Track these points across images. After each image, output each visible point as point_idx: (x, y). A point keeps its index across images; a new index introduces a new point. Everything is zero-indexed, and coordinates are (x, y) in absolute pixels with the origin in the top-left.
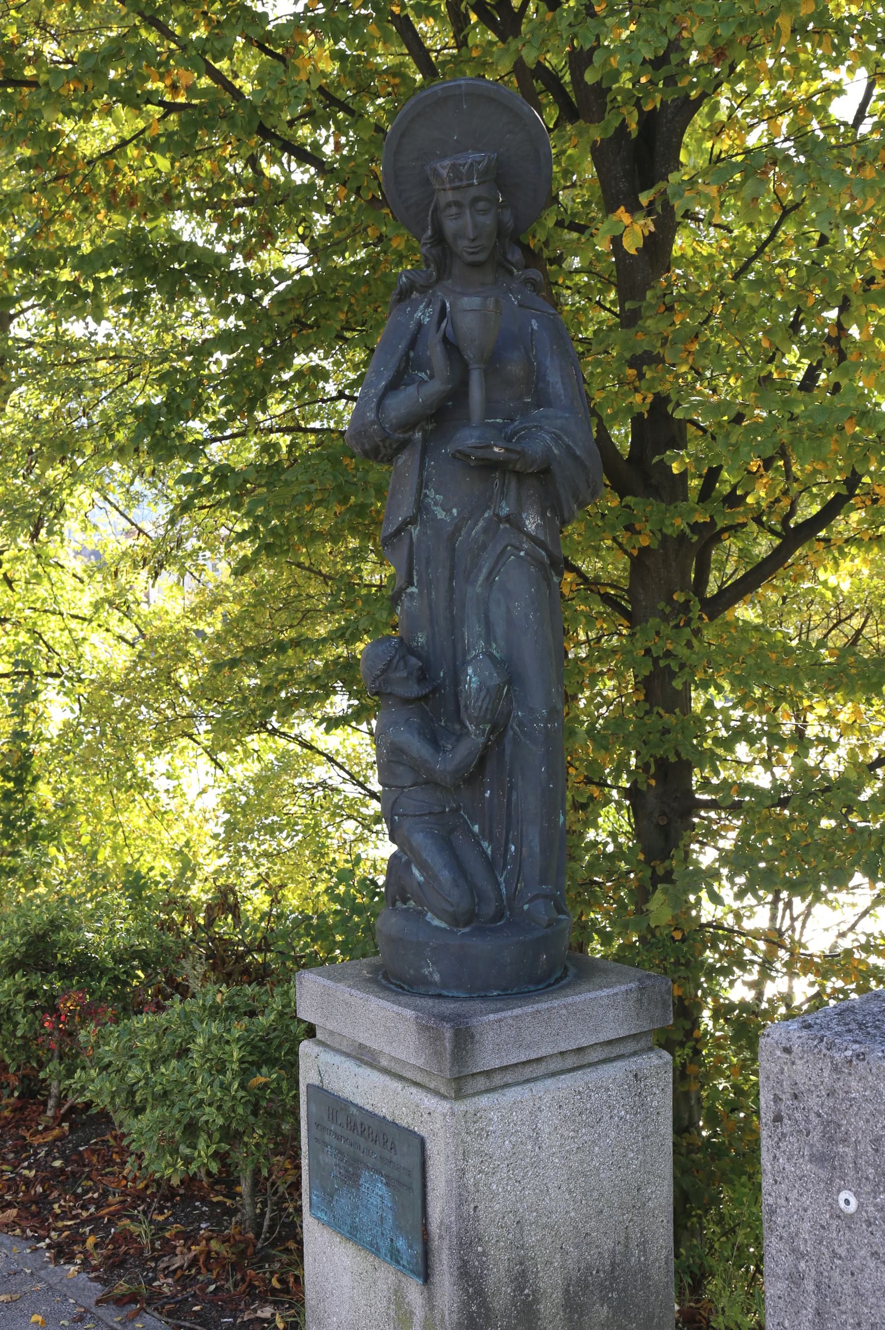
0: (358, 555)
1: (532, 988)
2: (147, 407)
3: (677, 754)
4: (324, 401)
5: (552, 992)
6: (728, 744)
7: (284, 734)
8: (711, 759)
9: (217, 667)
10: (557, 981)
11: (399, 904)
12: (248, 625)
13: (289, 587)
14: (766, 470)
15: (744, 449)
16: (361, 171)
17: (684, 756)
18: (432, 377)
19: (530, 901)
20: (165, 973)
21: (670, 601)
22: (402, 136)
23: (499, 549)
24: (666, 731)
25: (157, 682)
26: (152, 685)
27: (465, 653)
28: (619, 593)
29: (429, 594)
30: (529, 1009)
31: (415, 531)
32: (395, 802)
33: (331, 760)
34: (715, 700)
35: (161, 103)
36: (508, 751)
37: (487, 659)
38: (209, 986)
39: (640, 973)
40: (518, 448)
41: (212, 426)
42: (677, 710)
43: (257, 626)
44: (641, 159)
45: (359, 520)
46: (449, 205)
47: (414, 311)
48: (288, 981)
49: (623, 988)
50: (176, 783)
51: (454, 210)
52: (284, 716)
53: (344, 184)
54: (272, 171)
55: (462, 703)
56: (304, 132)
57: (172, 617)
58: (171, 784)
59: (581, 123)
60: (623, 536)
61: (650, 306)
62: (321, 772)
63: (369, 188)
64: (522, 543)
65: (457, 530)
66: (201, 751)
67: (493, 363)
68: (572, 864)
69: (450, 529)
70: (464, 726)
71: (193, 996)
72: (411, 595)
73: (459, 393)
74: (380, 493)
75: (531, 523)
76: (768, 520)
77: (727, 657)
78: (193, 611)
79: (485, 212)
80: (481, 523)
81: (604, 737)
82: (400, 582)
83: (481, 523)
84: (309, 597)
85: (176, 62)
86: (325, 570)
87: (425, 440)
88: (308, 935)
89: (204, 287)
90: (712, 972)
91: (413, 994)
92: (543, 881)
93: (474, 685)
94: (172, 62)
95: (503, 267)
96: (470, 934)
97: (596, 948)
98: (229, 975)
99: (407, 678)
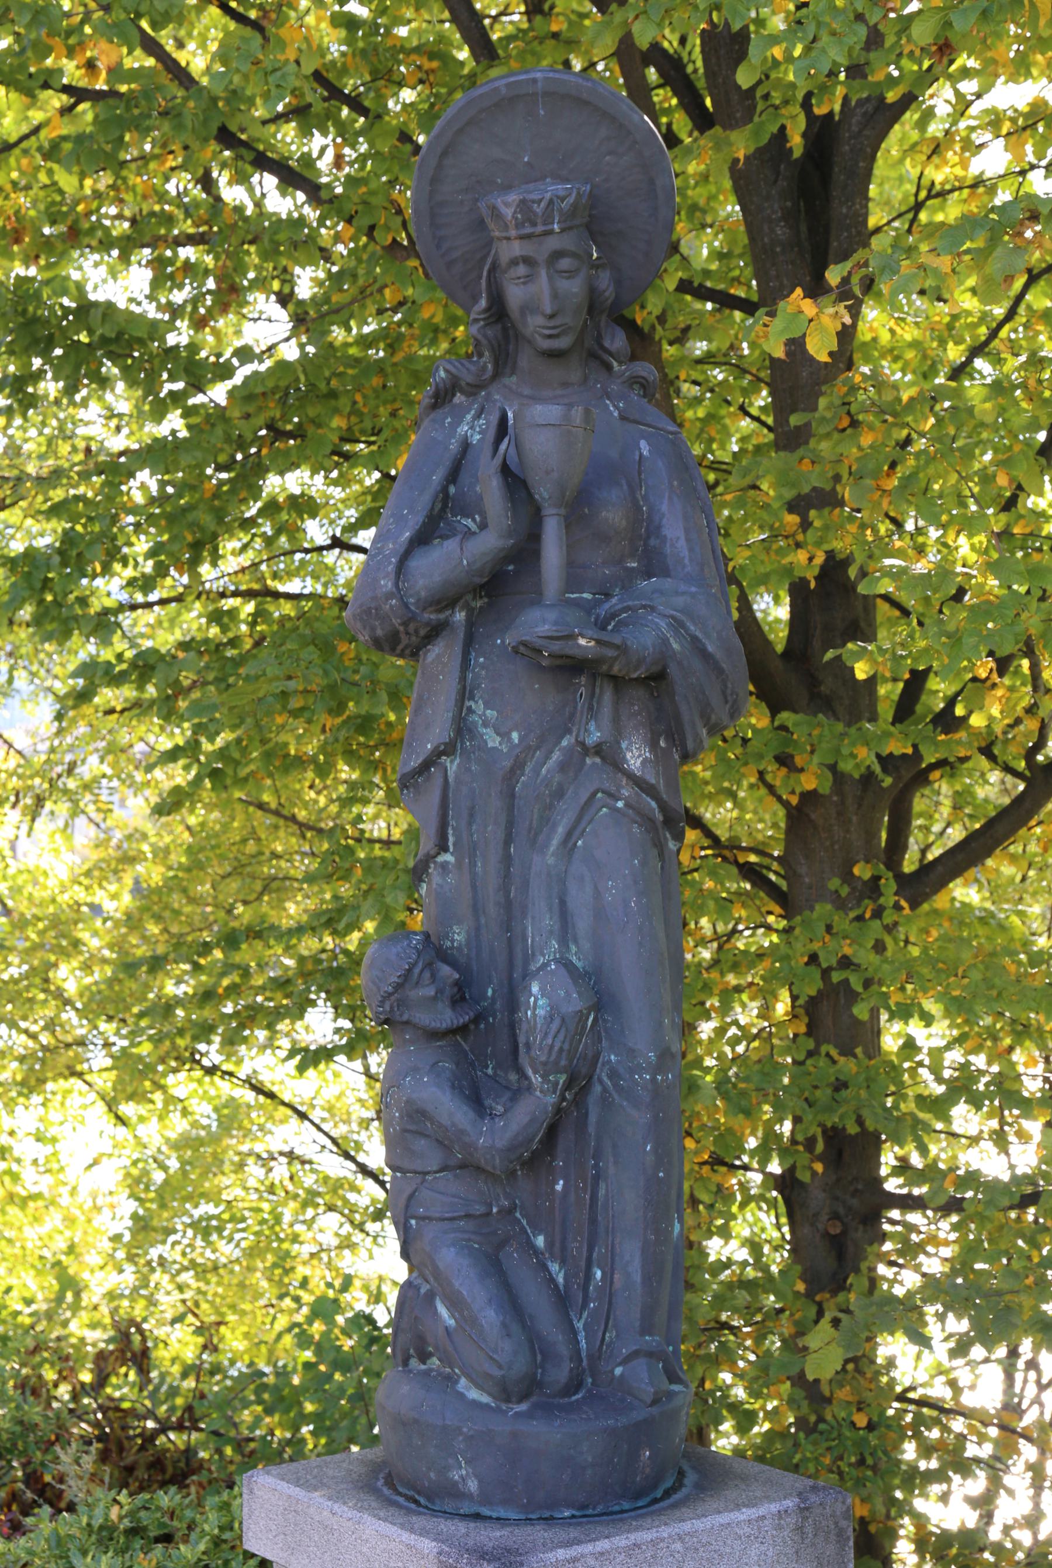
0: (356, 794)
1: (626, 1506)
2: (30, 554)
3: (860, 1121)
4: (307, 551)
5: (659, 1512)
6: (940, 1106)
7: (231, 1074)
8: (915, 1130)
9: (128, 967)
10: (667, 1494)
11: (414, 1363)
12: (176, 900)
13: (244, 841)
14: (1001, 675)
15: (969, 641)
16: (377, 201)
17: (870, 1125)
18: (483, 526)
19: (625, 1361)
20: (24, 1466)
21: (848, 876)
22: (445, 154)
23: (584, 796)
24: (840, 1085)
25: (27, 989)
26: (19, 993)
27: (527, 959)
28: (766, 861)
29: (473, 864)
30: (621, 1541)
31: (452, 765)
32: (412, 1196)
33: (303, 1116)
34: (922, 1037)
35: (67, 89)
36: (593, 1118)
37: (563, 971)
38: (99, 1492)
39: (802, 1483)
40: (617, 641)
41: (131, 583)
42: (859, 1051)
43: (191, 900)
44: (813, 204)
45: (362, 738)
46: (514, 262)
47: (458, 422)
48: (231, 1486)
49: (774, 1507)
50: (49, 1149)
51: (522, 270)
52: (231, 1041)
53: (349, 221)
54: (232, 194)
55: (522, 1040)
56: (287, 137)
57: (52, 883)
58: (42, 1151)
59: (717, 130)
60: (777, 776)
61: (823, 419)
62: (290, 1135)
63: (387, 228)
64: (619, 787)
65: (518, 766)
66: (93, 1096)
67: (579, 507)
68: (689, 1296)
69: (507, 764)
70: (524, 1076)
71: (71, 1508)
72: (444, 866)
73: (525, 552)
74: (396, 698)
75: (635, 757)
76: (1004, 751)
77: (939, 969)
78: (88, 874)
79: (570, 274)
80: (556, 756)
81: (743, 1094)
82: (427, 844)
83: (556, 756)
84: (275, 856)
85: (94, 29)
86: (302, 815)
87: (471, 624)
88: (259, 1402)
89: (126, 371)
90: (916, 1480)
91: (435, 1513)
92: (647, 1328)
93: (540, 1012)
94: (88, 30)
95: (597, 357)
96: (529, 1415)
97: (725, 1440)
98: (130, 1470)
99: (435, 998)
